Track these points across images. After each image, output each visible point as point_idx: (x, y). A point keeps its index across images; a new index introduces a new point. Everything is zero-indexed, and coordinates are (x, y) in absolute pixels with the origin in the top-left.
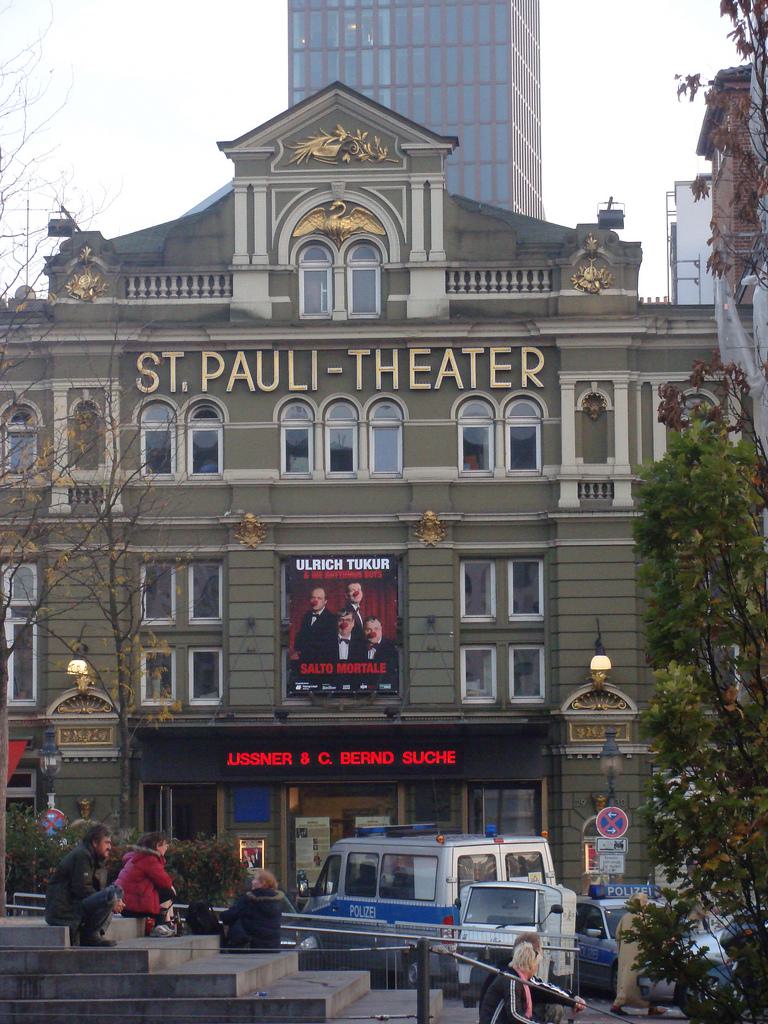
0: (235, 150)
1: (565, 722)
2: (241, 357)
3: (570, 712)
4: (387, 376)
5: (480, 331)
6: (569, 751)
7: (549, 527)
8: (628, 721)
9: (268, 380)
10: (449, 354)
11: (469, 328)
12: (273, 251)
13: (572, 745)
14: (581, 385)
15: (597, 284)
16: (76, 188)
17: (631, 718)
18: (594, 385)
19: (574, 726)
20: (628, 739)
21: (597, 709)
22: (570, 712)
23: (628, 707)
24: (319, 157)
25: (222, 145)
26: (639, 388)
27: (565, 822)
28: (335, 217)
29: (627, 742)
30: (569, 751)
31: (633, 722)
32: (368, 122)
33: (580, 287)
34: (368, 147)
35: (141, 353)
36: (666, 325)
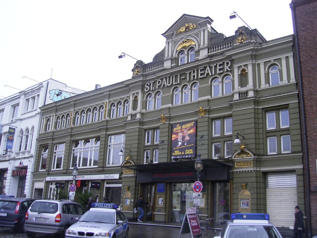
0: (167, 34)
1: (234, 162)
2: (164, 80)
3: (235, 159)
4: (194, 76)
5: (213, 59)
6: (235, 170)
7: (231, 107)
8: (252, 160)
9: (169, 83)
10: (208, 68)
11: (209, 59)
12: (172, 55)
13: (236, 168)
14: (239, 67)
15: (242, 41)
16: (120, 57)
17: (253, 159)
18: (243, 66)
19: (237, 163)
20: (252, 166)
21: (242, 157)
22: (235, 159)
23: (251, 156)
24: (182, 32)
25: (162, 35)
26: (257, 65)
27: (234, 192)
28: (185, 43)
29: (252, 167)
30: (235, 170)
31: (253, 160)
32: (193, 21)
33: (238, 42)
34: (192, 26)
35: (146, 84)
36: (260, 45)
